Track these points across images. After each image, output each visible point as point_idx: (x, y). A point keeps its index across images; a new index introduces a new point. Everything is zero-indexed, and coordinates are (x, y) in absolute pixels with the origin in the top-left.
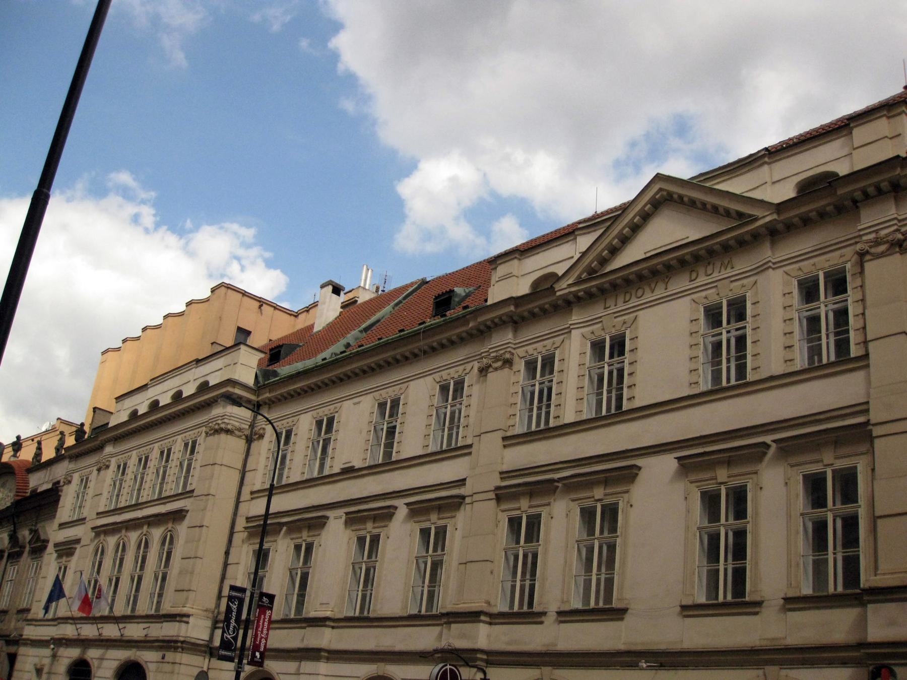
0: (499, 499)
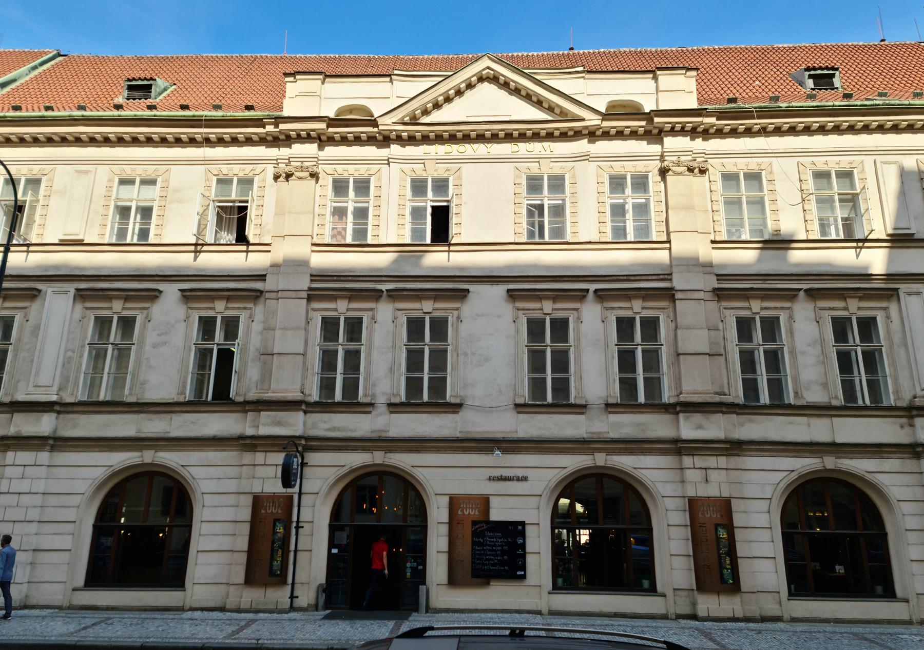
0: (310, 299)
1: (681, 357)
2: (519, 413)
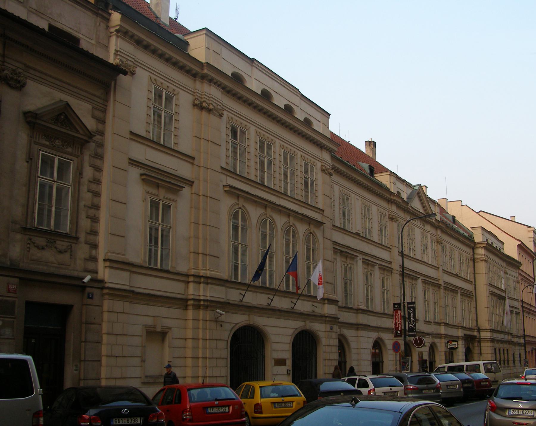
2: (425, 324)
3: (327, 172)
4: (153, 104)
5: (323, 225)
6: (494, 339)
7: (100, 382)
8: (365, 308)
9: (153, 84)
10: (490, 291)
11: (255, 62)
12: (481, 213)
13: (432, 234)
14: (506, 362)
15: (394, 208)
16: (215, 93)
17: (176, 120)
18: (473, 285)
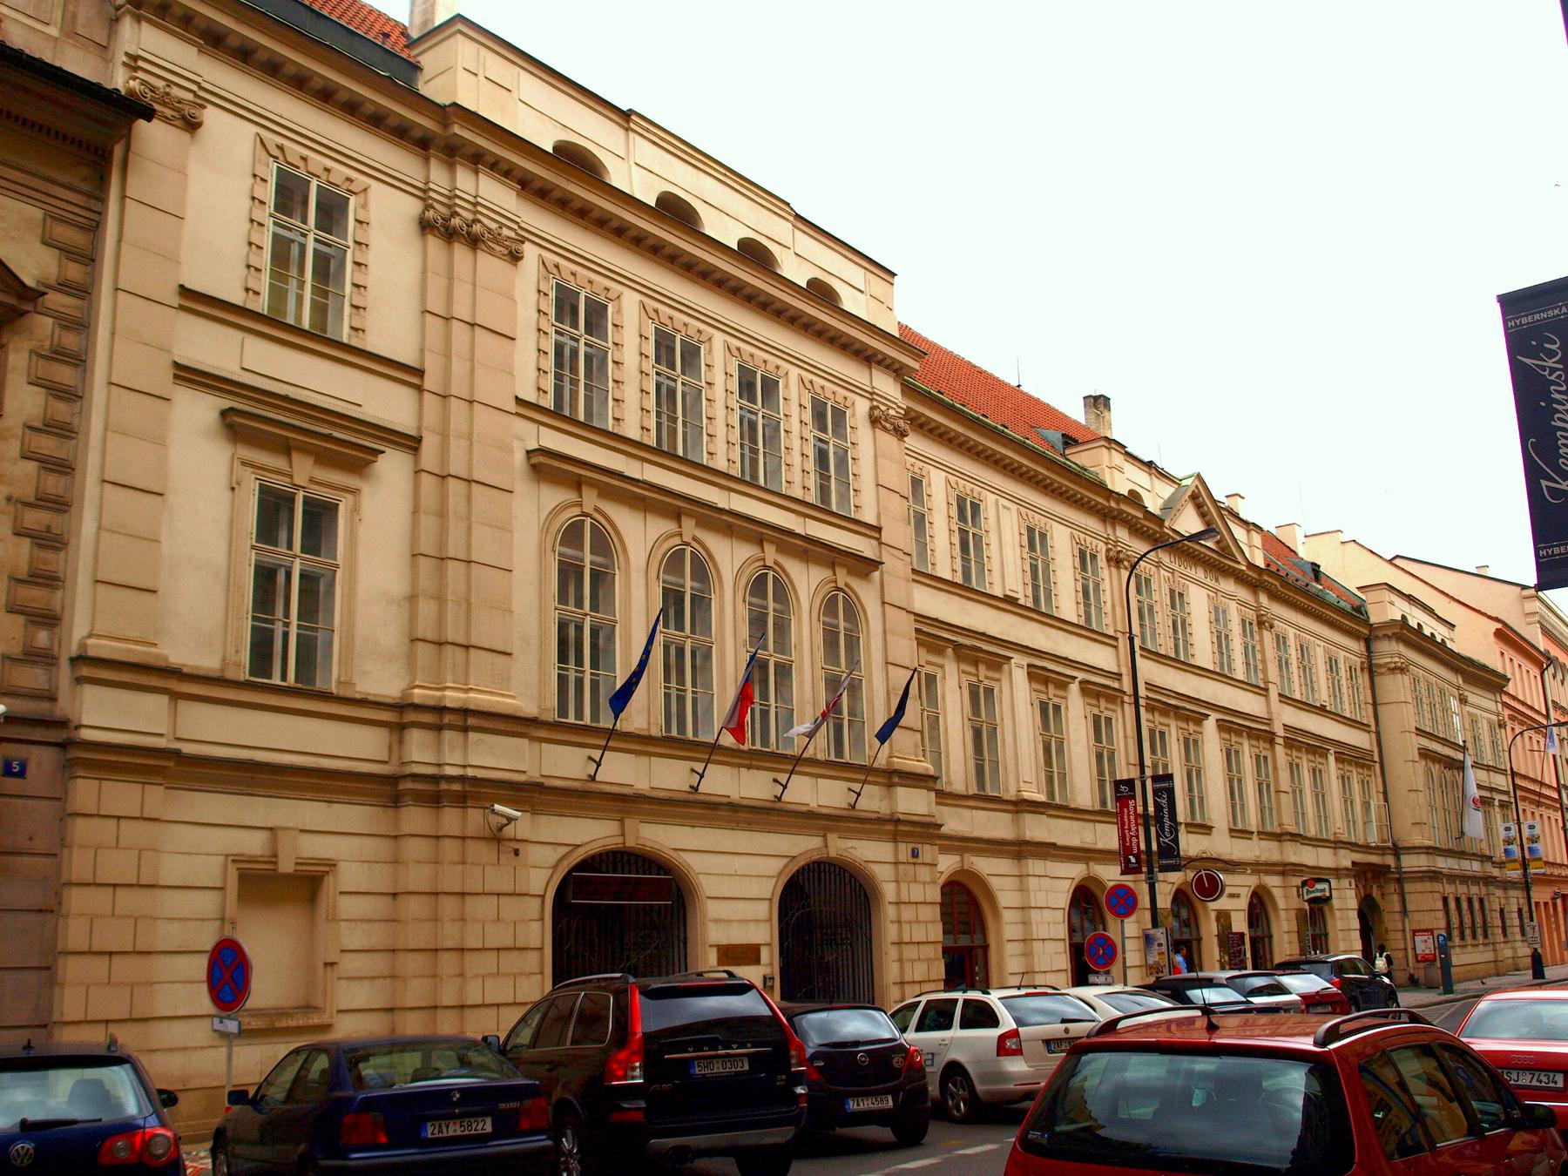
1: (1282, 794)
2: (1232, 837)
3: (888, 425)
4: (271, 215)
5: (876, 568)
6: (1440, 872)
7: (50, 1036)
8: (1042, 798)
9: (272, 159)
10: (1419, 749)
11: (633, 117)
12: (1397, 562)
13: (1241, 603)
14: (1479, 931)
15: (1122, 534)
16: (497, 195)
17: (358, 264)
18: (1373, 735)
